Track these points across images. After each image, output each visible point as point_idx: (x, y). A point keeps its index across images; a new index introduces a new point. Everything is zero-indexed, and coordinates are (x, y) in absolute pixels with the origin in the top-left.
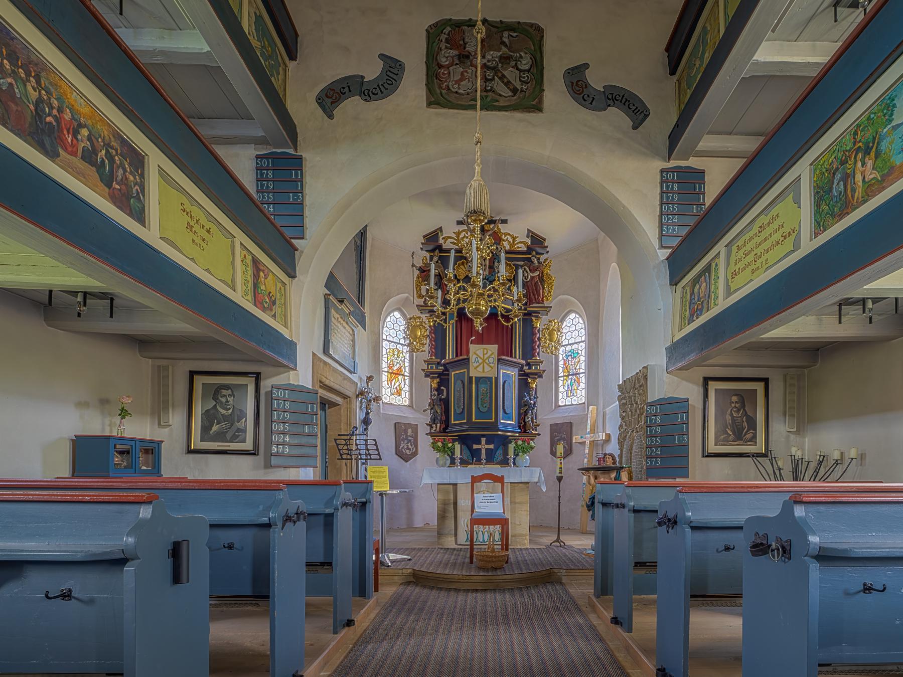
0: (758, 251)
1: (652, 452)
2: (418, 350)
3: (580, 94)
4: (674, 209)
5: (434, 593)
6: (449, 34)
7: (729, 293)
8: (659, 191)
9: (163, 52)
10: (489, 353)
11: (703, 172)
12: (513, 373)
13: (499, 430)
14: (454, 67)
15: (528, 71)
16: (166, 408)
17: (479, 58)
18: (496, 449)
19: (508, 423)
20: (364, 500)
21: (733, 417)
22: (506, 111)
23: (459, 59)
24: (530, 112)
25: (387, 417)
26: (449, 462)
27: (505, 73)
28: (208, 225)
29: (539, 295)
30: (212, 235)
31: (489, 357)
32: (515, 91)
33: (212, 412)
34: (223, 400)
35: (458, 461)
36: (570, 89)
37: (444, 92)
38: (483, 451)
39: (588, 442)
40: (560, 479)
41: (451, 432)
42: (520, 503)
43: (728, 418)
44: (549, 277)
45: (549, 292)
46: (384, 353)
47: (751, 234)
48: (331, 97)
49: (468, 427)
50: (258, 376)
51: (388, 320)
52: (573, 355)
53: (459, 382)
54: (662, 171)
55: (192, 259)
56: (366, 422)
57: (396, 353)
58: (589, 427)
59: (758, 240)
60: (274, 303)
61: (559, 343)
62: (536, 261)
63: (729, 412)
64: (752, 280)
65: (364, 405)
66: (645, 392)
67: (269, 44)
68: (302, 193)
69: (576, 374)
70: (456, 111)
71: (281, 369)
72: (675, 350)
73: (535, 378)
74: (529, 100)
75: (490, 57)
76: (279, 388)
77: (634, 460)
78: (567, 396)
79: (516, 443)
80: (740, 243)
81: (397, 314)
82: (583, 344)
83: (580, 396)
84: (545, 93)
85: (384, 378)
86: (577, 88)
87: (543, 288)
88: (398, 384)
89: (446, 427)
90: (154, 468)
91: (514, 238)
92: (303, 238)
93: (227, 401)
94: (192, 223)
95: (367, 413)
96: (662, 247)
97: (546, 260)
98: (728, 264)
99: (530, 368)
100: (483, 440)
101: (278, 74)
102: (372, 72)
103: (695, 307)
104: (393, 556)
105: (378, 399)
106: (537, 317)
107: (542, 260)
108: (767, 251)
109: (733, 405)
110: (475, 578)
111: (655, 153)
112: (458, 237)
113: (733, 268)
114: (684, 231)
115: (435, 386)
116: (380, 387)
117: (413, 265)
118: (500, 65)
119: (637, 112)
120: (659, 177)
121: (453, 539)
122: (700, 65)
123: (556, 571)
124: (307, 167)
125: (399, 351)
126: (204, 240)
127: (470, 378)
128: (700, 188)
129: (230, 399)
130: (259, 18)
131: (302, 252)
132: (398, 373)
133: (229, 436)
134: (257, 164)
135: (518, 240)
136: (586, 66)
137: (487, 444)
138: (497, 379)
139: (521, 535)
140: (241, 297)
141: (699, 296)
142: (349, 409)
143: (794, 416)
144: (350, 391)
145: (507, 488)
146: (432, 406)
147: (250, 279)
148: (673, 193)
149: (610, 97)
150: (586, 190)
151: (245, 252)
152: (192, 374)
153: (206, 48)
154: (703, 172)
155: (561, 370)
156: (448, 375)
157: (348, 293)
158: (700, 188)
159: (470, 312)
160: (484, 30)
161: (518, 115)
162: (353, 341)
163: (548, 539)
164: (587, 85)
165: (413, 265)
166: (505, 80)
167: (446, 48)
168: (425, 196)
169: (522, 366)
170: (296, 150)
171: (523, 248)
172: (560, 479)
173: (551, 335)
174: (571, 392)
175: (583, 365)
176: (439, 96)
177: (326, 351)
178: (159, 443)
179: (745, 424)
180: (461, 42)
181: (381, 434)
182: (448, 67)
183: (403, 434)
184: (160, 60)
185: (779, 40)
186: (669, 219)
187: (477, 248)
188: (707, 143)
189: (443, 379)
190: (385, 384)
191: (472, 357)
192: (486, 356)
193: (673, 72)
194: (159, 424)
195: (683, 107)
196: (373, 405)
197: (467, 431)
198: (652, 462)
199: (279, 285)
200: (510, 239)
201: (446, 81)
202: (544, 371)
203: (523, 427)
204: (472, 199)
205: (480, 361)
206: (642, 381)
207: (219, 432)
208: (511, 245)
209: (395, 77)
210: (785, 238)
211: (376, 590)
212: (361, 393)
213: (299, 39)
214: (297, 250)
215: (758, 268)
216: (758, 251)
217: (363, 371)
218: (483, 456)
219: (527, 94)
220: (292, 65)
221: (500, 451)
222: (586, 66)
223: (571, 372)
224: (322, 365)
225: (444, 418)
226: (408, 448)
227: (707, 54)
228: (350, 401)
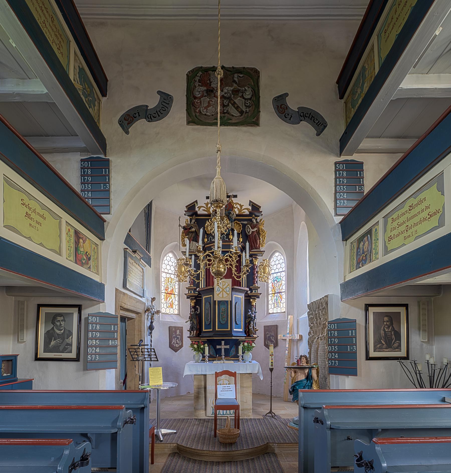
0: (409, 223)
1: (332, 356)
2: (182, 280)
3: (283, 113)
4: (344, 189)
5: (191, 465)
6: (200, 77)
7: (386, 251)
8: (334, 177)
9: (19, 94)
10: (227, 284)
11: (362, 163)
12: (241, 296)
14: (204, 98)
15: (250, 99)
16: (22, 330)
17: (219, 91)
18: (231, 347)
19: (238, 330)
20: (143, 406)
21: (384, 330)
22: (236, 126)
23: (207, 93)
24: (251, 126)
25: (164, 323)
26: (201, 358)
27: (236, 101)
28: (42, 212)
29: (257, 244)
30: (45, 219)
31: (226, 287)
32: (242, 112)
33: (51, 332)
34: (58, 324)
35: (207, 359)
36: (277, 110)
37: (197, 114)
38: (223, 350)
39: (288, 340)
40: (271, 370)
42: (246, 387)
43: (382, 332)
44: (263, 231)
45: (263, 241)
46: (163, 280)
47: (403, 210)
48: (127, 120)
49: (215, 332)
50: (79, 307)
51: (165, 259)
52: (276, 280)
53: (208, 303)
54: (336, 163)
55: (29, 238)
56: (151, 328)
57: (170, 280)
58: (288, 330)
59: (408, 215)
60: (89, 259)
61: (269, 274)
62: (255, 221)
63: (382, 328)
64: (404, 245)
65: (150, 317)
66: (326, 313)
67: (88, 87)
68: (109, 183)
69: (279, 293)
70: (205, 127)
71: (95, 302)
72: (348, 288)
73: (255, 299)
74: (250, 118)
75: (226, 91)
76: (93, 315)
77: (319, 359)
78: (274, 307)
79: (243, 344)
80: (395, 216)
81: (171, 255)
82: (284, 273)
83: (283, 308)
84: (261, 114)
85: (163, 297)
86: (281, 110)
87: (260, 239)
88: (171, 300)
89: (199, 335)
90: (12, 374)
91: (241, 206)
92: (109, 214)
93: (61, 325)
94: (30, 212)
95: (152, 322)
96: (336, 215)
97: (261, 220)
98: (385, 231)
100: (223, 342)
101: (94, 106)
102: (153, 102)
103: (361, 258)
104: (164, 431)
105: (158, 312)
107: (258, 221)
108: (416, 225)
109: (385, 323)
110: (218, 453)
111: (331, 151)
112: (207, 206)
113: (389, 234)
114: (354, 204)
115: (193, 304)
116: (159, 303)
117: (180, 226)
118: (232, 96)
119: (319, 124)
120: (334, 167)
121: (204, 412)
122: (361, 92)
123: (271, 444)
124: (113, 166)
126: (38, 223)
127: (215, 302)
128: (360, 174)
129: (63, 323)
130: (81, 70)
131: (109, 223)
133: (61, 348)
134: (82, 165)
135: (243, 207)
136: (287, 95)
137: (225, 349)
138: (231, 302)
139: (247, 410)
140: (66, 260)
141: (363, 250)
142: (140, 321)
143: (426, 331)
144: (140, 309)
145: (238, 376)
146: (191, 318)
147: (73, 245)
148: (343, 178)
149: (302, 115)
150: (288, 177)
151: (69, 227)
152: (39, 306)
153: (46, 91)
154: (362, 163)
155: (270, 289)
156: (201, 297)
157: (139, 246)
158: (360, 174)
159: (213, 273)
160: (222, 73)
161: (244, 128)
162: (143, 276)
163: (265, 410)
164: (287, 107)
165: (180, 226)
166: (236, 106)
167: (199, 85)
168: (188, 182)
169: (247, 291)
170: (105, 155)
171: (247, 212)
172: (271, 370)
173: (264, 269)
174: (277, 304)
175: (284, 287)
176: (195, 117)
177: (124, 286)
178: (16, 356)
179: (393, 336)
180: (208, 82)
181: (158, 340)
182: (200, 98)
183: (174, 333)
184: (17, 99)
185: (416, 73)
186: (341, 196)
187: (218, 227)
188: (366, 144)
190: (163, 301)
192: (224, 287)
193: (341, 97)
194: (18, 341)
195: (349, 121)
196: (156, 316)
197: (212, 337)
198: (332, 363)
199: (93, 246)
200: (239, 207)
201: (199, 107)
202: (261, 294)
203: (248, 332)
204: (215, 192)
205: (221, 290)
206: (324, 305)
207: (55, 348)
208: (240, 211)
209: (167, 105)
210: (431, 216)
211: (152, 463)
212: (148, 310)
213: (108, 83)
214: (105, 221)
215: (409, 236)
216: (409, 223)
217: (149, 295)
218: (223, 353)
219: (249, 114)
220: (104, 100)
221: (233, 349)
222: (287, 95)
223: (277, 292)
224: (122, 295)
225: (198, 327)
226: (177, 343)
227: (365, 85)
228: (141, 316)
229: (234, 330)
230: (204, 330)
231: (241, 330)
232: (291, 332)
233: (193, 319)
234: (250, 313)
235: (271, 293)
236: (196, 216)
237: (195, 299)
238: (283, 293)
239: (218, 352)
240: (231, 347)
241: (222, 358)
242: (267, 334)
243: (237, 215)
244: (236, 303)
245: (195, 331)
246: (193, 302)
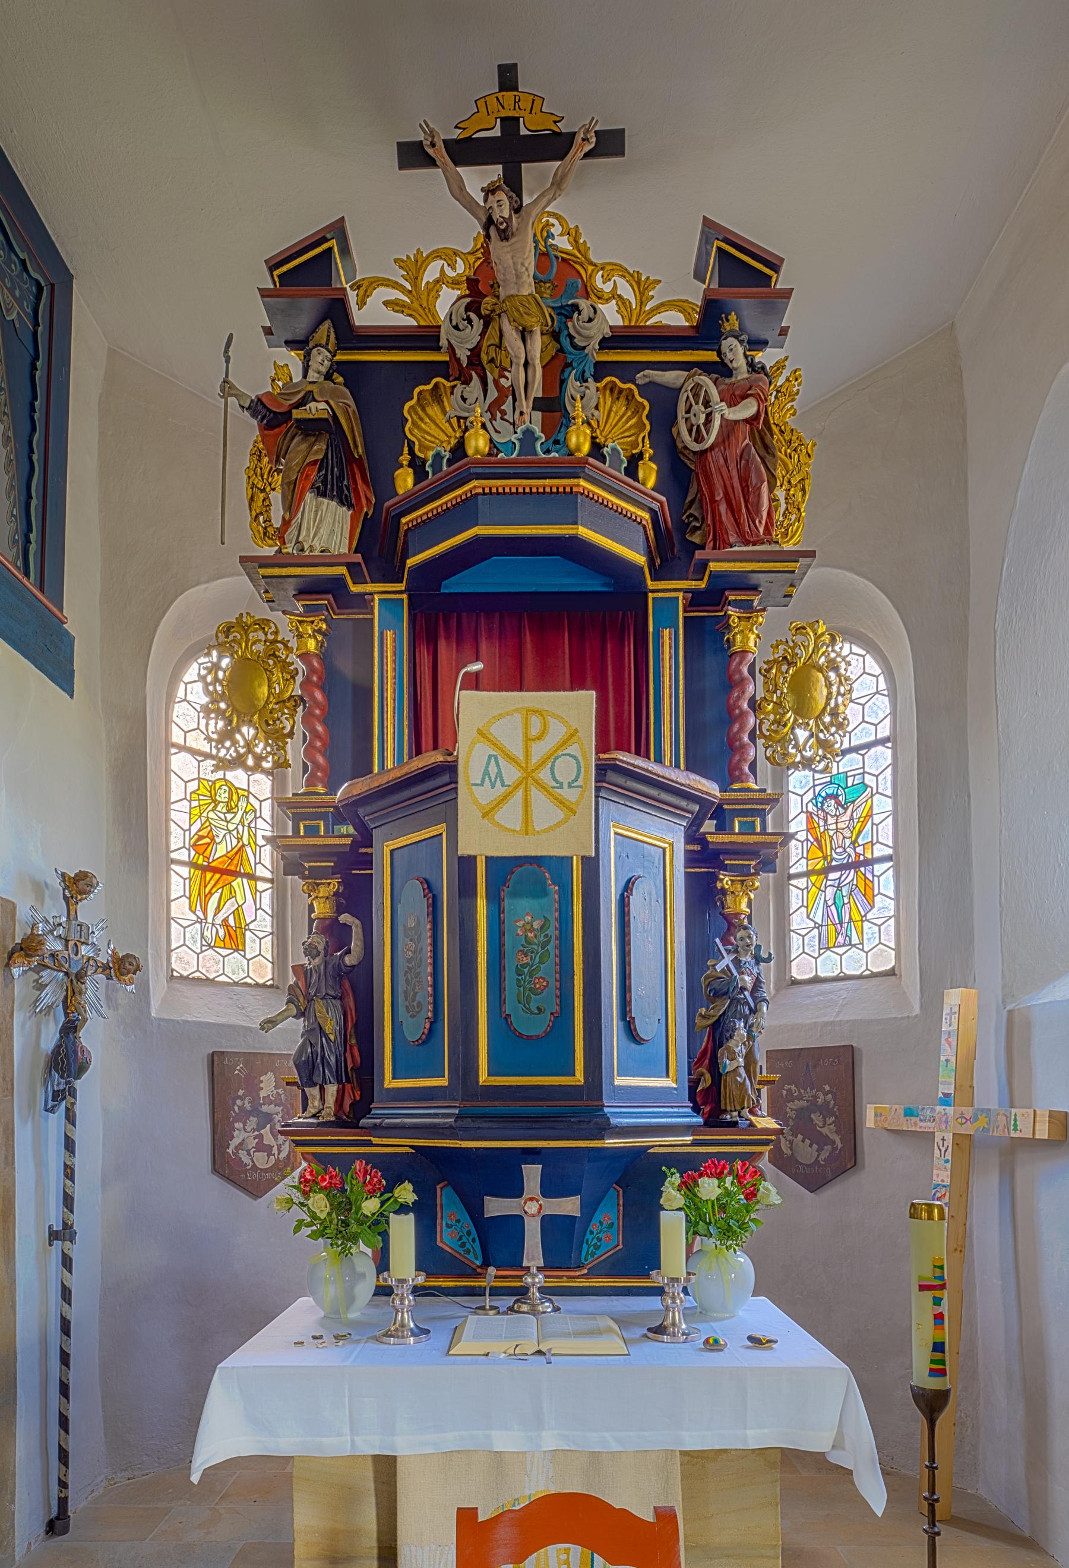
10: (557, 732)
12: (664, 837)
13: (604, 1129)
19: (645, 1090)
25: (179, 1034)
31: (553, 756)
39: (944, 1137)
40: (932, 1404)
41: (375, 1129)
56: (66, 1063)
57: (223, 796)
69: (855, 865)
73: (744, 872)
83: (877, 942)
85: (177, 886)
89: (352, 1116)
95: (70, 1029)
99: (721, 828)
106: (746, 606)
115: (322, 909)
125: (232, 789)
127: (466, 864)
132: (229, 871)
137: (549, 1223)
138: (591, 866)
172: (932, 1404)
174: (837, 931)
175: (886, 832)
189: (352, 879)
190: (180, 908)
191: (472, 758)
192: (539, 751)
200: (626, 290)
205: (512, 774)
223: (839, 859)
226: (261, 1147)
229: (619, 1081)
230: (389, 1083)
231: (669, 1083)
232: (965, 1090)
233: (319, 1006)
234: (727, 960)
235: (801, 867)
236: (341, 347)
237: (334, 872)
238: (879, 868)
239: (499, 1242)
240: (590, 1208)
241: (522, 1292)
242: (790, 1098)
243: (615, 340)
244: (628, 887)
245: (332, 1090)
246: (323, 891)
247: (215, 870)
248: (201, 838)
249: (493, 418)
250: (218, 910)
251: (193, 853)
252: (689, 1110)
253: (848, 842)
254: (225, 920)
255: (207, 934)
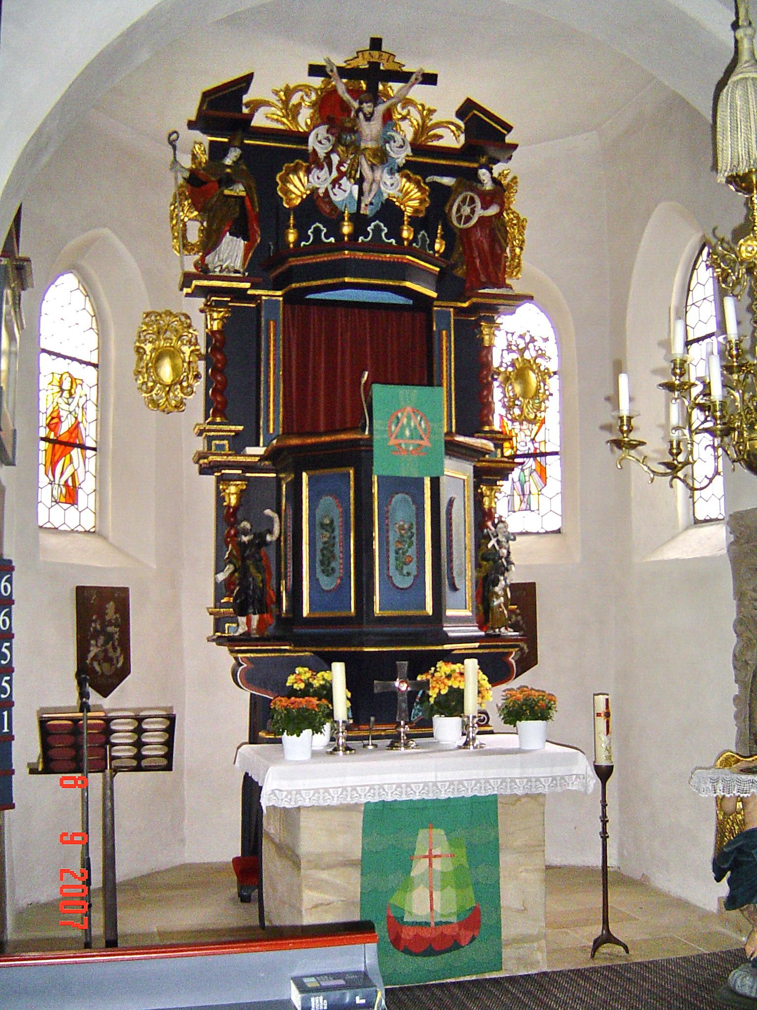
57: (66, 385)
66: (379, 949)
135: (435, 118)
247: (61, 443)
248: (53, 418)
249: (334, 187)
250: (62, 474)
251: (48, 430)
252: (476, 628)
253: (528, 439)
254: (66, 482)
255: (55, 493)
